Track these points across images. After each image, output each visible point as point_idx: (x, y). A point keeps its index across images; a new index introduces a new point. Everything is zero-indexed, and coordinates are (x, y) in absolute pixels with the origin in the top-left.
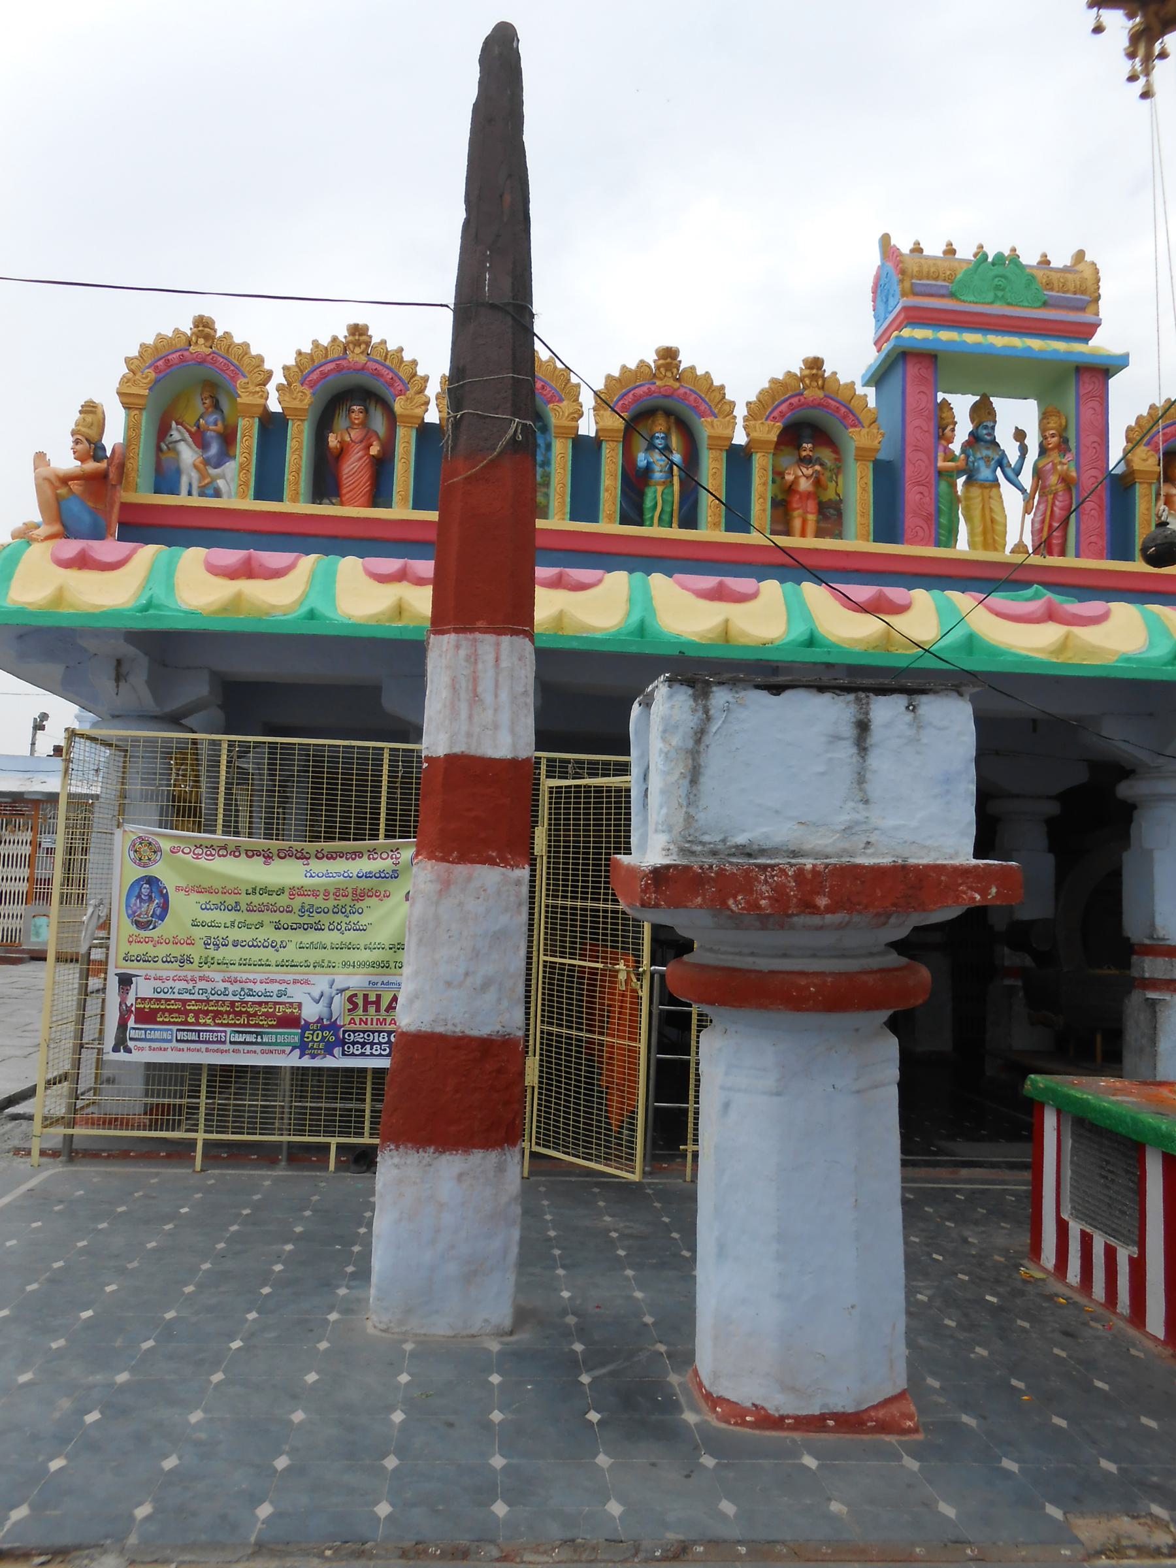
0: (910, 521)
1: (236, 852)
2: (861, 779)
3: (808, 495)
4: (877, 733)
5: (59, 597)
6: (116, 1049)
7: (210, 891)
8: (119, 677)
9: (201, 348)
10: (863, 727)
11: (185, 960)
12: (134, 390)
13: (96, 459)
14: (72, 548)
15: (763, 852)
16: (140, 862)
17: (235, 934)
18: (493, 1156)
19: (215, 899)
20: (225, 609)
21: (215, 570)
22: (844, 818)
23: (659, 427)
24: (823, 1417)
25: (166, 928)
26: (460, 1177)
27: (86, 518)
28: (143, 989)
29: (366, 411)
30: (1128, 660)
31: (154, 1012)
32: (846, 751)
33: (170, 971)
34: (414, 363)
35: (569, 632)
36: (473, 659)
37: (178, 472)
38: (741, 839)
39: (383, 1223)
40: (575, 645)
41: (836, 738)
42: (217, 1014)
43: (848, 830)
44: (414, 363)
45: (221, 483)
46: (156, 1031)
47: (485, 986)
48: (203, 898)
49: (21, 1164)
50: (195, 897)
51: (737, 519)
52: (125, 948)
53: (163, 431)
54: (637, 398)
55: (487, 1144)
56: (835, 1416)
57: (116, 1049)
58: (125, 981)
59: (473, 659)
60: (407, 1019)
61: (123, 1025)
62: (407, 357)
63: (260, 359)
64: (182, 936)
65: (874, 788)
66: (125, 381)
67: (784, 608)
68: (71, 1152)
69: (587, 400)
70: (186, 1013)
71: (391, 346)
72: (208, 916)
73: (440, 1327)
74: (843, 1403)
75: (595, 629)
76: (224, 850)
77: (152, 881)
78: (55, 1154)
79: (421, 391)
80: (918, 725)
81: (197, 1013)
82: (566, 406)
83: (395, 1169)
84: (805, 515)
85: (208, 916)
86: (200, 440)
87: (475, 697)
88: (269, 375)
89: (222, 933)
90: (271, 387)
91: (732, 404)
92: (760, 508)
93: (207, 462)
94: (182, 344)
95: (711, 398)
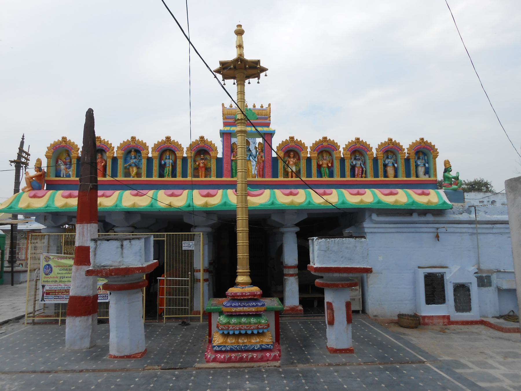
0: (225, 172)
1: (66, 258)
2: (122, 254)
3: (202, 167)
4: (124, 247)
5: (28, 206)
6: (42, 301)
7: (61, 266)
8: (45, 220)
9: (63, 144)
10: (122, 245)
11: (56, 281)
12: (49, 155)
13: (40, 172)
14: (33, 193)
15: (106, 266)
16: (46, 261)
17: (66, 275)
18: (86, 317)
19: (62, 268)
20: (63, 206)
21: (64, 197)
22: (119, 260)
23: (168, 154)
24: (124, 356)
25: (52, 275)
26: (80, 321)
27: (37, 185)
28: (47, 288)
29: (102, 155)
30: (261, 205)
31: (49, 293)
32: (120, 249)
33: (52, 284)
34: (111, 144)
35: (136, 207)
36: (83, 228)
37: (61, 171)
38: (103, 264)
39: (67, 330)
40: (136, 210)
41: (118, 248)
42: (62, 292)
43: (120, 262)
44: (111, 144)
45: (70, 173)
46: (50, 296)
47: (85, 287)
48: (59, 268)
49: (23, 326)
50: (58, 268)
51: (184, 175)
52: (43, 279)
53: (57, 162)
54: (161, 149)
55: (85, 315)
56: (126, 356)
57: (42, 301)
58: (43, 286)
59: (83, 228)
60: (71, 294)
61: (43, 296)
62: (109, 143)
63: (77, 145)
64: (55, 276)
65: (124, 255)
66: (47, 152)
67: (186, 197)
68: (34, 323)
69: (150, 150)
70: (56, 292)
71: (106, 141)
72: (61, 272)
73: (76, 348)
74: (127, 353)
75: (142, 206)
76: (63, 258)
77: (49, 265)
78: (31, 324)
79: (113, 150)
80: (131, 245)
81: (58, 293)
82: (145, 151)
83: (69, 320)
84: (202, 172)
85: (61, 272)
86: (65, 164)
87: (83, 235)
88: (79, 149)
89: (64, 275)
90: (79, 151)
91: (183, 148)
92: (189, 171)
93: (67, 168)
94: (59, 143)
95: (179, 147)
